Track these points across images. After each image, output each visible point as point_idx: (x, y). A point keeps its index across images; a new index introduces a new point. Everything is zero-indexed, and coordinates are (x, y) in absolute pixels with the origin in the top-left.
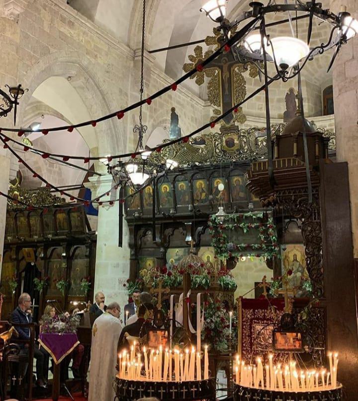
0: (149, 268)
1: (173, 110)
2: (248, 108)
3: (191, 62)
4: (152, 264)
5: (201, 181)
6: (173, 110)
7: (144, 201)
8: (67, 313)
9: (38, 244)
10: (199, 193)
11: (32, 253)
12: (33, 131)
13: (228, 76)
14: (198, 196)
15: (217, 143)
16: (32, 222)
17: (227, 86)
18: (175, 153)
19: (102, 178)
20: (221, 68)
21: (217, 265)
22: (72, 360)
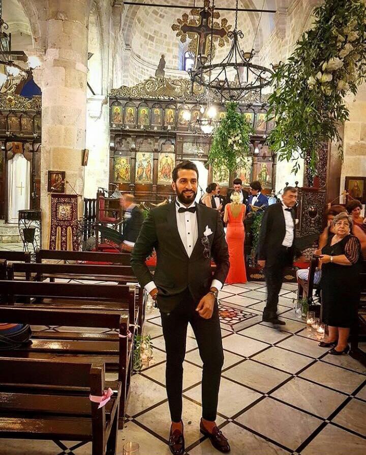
0: (122, 163)
1: (163, 56)
2: (144, 56)
3: (178, 24)
4: (125, 162)
5: (158, 110)
6: (163, 56)
7: (126, 118)
8: (225, 230)
9: (28, 140)
10: (168, 118)
11: (21, 146)
12: (226, 79)
13: (204, 41)
14: (167, 120)
15: (189, 86)
16: (23, 122)
17: (202, 48)
18: (157, 88)
19: (95, 97)
20: (200, 34)
21: (173, 165)
22: (154, 249)
